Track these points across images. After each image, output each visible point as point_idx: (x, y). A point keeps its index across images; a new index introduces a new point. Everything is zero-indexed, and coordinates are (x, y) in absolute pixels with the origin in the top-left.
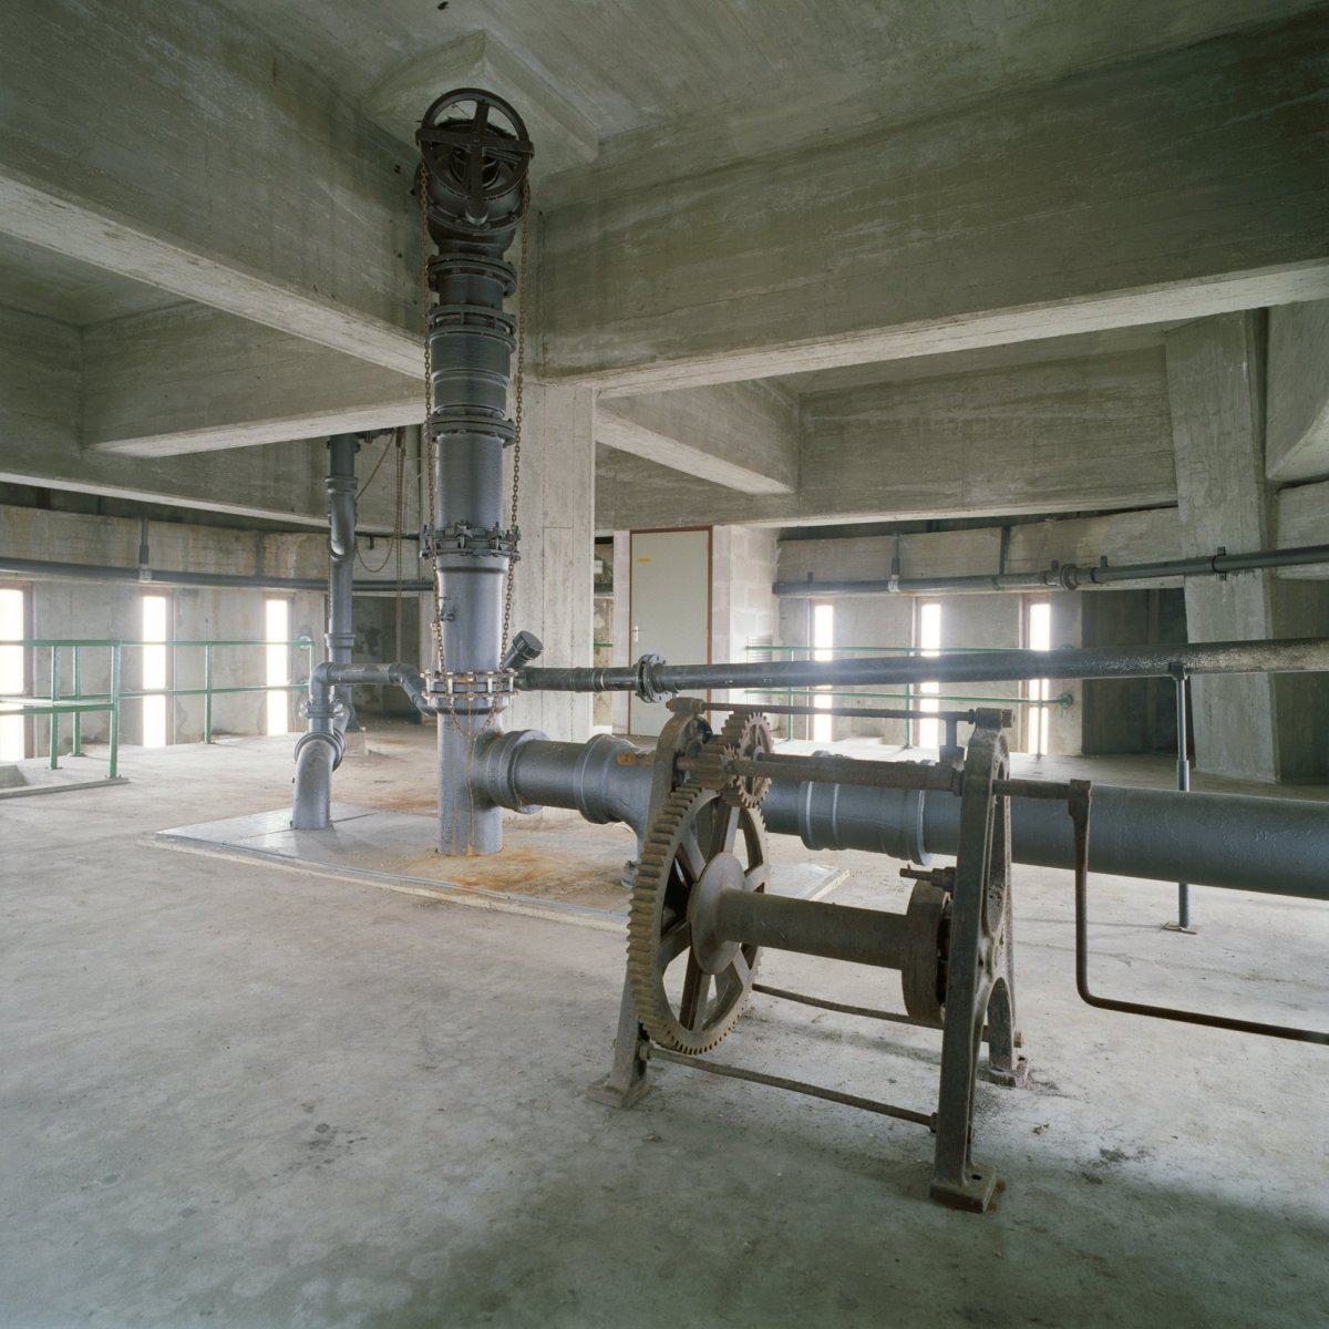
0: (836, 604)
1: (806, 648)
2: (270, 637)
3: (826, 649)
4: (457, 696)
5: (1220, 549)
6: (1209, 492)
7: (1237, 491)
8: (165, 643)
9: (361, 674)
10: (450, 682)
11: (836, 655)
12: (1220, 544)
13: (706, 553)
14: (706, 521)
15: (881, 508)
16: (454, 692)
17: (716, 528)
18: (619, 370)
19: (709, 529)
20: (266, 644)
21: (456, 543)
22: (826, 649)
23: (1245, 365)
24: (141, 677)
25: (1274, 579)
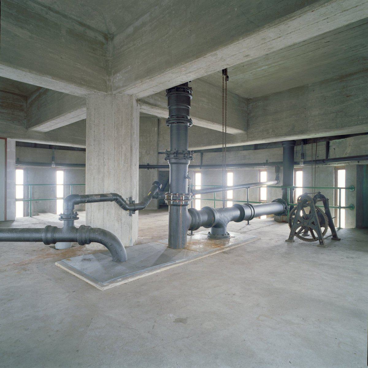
0: (24, 169)
1: (65, 185)
2: (58, 183)
3: (58, 185)
4: (173, 201)
5: (148, 164)
6: (146, 152)
7: (152, 153)
8: (195, 186)
9: (99, 198)
10: (172, 196)
11: (201, 187)
12: (148, 162)
13: (4, 148)
14: (5, 135)
15: (70, 142)
16: (173, 199)
17: (8, 139)
18: (159, 108)
19: (6, 139)
20: (201, 186)
21: (174, 155)
22: (58, 185)
23: (156, 129)
24: (15, 213)
25: (158, 170)
